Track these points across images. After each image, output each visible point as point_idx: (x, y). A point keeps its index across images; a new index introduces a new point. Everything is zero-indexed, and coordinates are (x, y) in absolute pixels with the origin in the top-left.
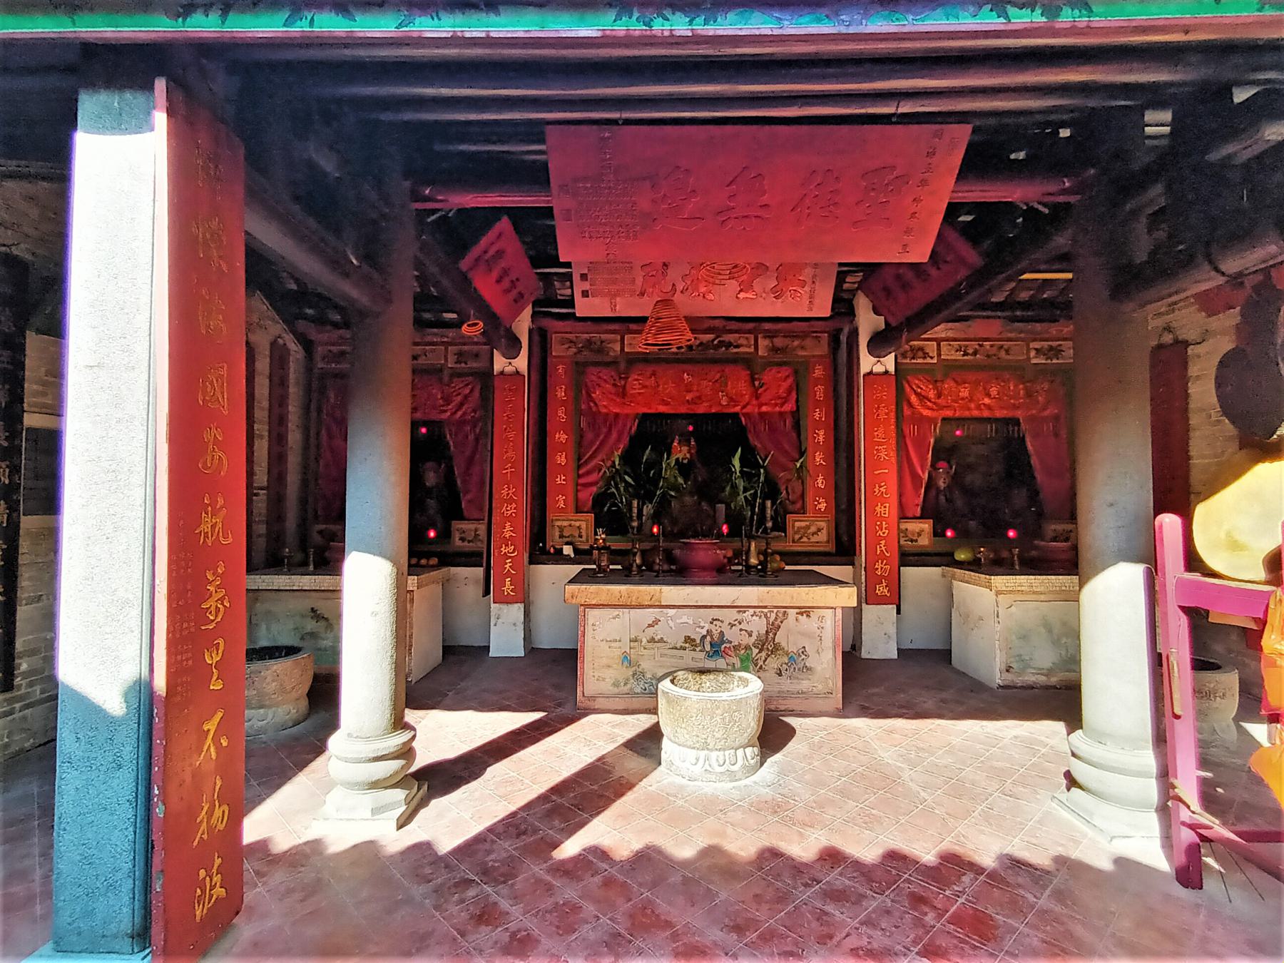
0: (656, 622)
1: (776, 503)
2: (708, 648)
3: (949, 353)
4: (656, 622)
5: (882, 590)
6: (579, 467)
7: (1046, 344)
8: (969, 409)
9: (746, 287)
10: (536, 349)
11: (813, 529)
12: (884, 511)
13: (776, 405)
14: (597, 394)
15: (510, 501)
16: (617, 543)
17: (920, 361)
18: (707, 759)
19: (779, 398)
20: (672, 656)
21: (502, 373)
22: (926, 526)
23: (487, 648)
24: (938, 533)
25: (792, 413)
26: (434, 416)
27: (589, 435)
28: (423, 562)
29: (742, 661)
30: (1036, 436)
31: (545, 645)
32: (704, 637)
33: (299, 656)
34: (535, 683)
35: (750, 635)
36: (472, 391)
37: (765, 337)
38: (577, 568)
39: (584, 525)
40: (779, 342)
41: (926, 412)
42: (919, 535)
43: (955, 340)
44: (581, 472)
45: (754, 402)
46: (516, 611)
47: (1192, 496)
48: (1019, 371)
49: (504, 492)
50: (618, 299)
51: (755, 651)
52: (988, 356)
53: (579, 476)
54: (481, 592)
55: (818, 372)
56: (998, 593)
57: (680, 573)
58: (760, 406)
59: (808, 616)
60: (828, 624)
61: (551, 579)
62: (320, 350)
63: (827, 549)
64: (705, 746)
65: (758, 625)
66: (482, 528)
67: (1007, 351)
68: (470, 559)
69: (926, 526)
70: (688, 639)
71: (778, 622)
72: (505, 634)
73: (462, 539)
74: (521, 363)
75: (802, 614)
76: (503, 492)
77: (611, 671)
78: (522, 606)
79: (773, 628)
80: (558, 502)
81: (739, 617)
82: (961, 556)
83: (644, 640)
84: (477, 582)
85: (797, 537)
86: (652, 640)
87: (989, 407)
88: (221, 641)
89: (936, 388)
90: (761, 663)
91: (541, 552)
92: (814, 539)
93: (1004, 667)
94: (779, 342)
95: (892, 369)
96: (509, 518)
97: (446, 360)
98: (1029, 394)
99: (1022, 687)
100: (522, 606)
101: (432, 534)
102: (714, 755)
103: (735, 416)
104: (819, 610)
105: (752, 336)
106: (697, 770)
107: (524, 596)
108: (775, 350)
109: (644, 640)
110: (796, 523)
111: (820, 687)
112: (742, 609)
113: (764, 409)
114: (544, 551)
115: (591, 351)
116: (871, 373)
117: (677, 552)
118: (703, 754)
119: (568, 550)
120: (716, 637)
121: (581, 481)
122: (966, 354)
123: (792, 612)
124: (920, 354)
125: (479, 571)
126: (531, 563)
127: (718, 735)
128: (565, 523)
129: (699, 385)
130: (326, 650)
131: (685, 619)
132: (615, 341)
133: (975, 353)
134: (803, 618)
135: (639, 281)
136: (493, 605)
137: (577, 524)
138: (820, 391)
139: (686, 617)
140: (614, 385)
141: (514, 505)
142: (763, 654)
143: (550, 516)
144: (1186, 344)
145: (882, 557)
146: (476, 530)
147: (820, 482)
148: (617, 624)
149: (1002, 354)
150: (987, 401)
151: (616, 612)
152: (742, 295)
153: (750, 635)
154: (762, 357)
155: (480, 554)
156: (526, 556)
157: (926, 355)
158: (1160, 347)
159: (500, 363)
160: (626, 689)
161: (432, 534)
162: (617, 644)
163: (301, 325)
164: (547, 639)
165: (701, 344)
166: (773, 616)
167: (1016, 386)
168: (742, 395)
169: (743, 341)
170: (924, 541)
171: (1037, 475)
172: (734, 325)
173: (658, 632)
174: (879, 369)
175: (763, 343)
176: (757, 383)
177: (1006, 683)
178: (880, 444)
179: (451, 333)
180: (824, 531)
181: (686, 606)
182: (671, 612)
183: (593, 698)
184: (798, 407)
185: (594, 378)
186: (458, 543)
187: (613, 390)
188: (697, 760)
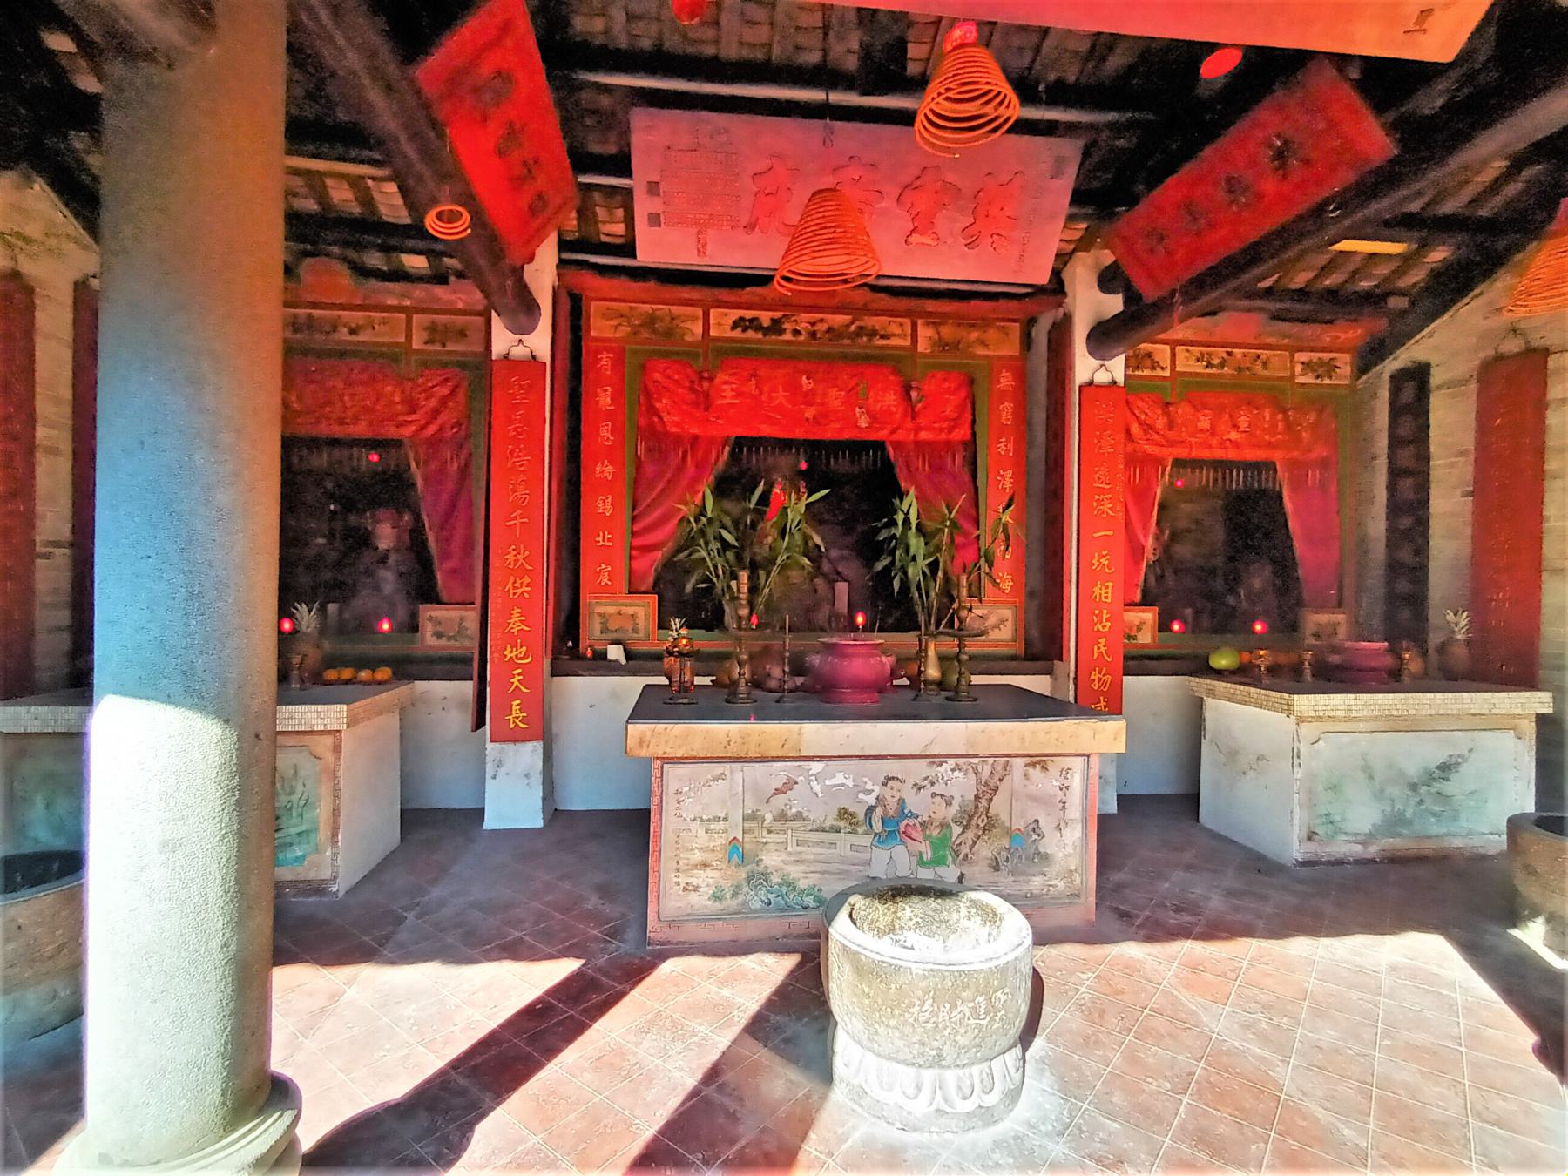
0: (790, 785)
2: (877, 826)
3: (1187, 362)
4: (790, 785)
6: (634, 519)
7: (1315, 356)
8: (1210, 447)
9: (922, 225)
10: (564, 324)
11: (993, 620)
12: (1104, 597)
13: (941, 430)
14: (663, 404)
16: (706, 641)
17: (1146, 372)
18: (940, 1086)
19: (946, 419)
20: (817, 844)
21: (506, 357)
22: (1148, 616)
23: (479, 813)
24: (1163, 626)
25: (964, 443)
26: (390, 431)
27: (649, 470)
28: (364, 675)
29: (935, 848)
30: (1297, 486)
31: (577, 805)
32: (871, 809)
34: (567, 885)
35: (949, 803)
36: (453, 392)
37: (928, 324)
38: (639, 682)
39: (641, 612)
40: (947, 331)
41: (1150, 449)
42: (1139, 629)
43: (1192, 343)
44: (637, 527)
45: (909, 424)
46: (529, 754)
47: (1545, 576)
48: (1274, 396)
50: (710, 231)
51: (957, 830)
53: (634, 534)
54: (469, 718)
55: (1006, 381)
56: (1301, 720)
57: (820, 695)
58: (918, 430)
60: (1076, 782)
61: (595, 702)
63: (1012, 651)
64: (938, 1062)
65: (961, 786)
66: (471, 617)
67: (1265, 364)
68: (449, 667)
69: (1148, 616)
70: (844, 814)
71: (992, 783)
72: (511, 797)
73: (439, 635)
74: (540, 342)
75: (1033, 765)
76: (506, 557)
77: (709, 872)
78: (539, 745)
79: (988, 791)
80: (598, 572)
81: (932, 772)
82: (1221, 661)
83: (769, 817)
84: (461, 705)
87: (1236, 445)
89: (1167, 414)
90: (965, 850)
91: (570, 649)
92: (994, 635)
93: (1304, 834)
94: (947, 331)
95: (1120, 379)
96: (520, 601)
97: (409, 336)
98: (1289, 427)
99: (1329, 863)
100: (539, 745)
101: (386, 626)
102: (951, 1076)
103: (879, 446)
104: (1070, 766)
105: (907, 322)
106: (920, 1107)
107: (541, 729)
108: (942, 345)
109: (769, 817)
111: (1061, 885)
112: (937, 759)
113: (923, 435)
114: (575, 654)
115: (654, 331)
116: (1091, 383)
117: (815, 660)
118: (928, 1075)
119: (615, 653)
120: (892, 807)
121: (638, 542)
123: (1020, 762)
124: (1148, 362)
125: (467, 688)
126: (555, 673)
127: (962, 1040)
128: (611, 610)
129: (825, 394)
131: (840, 778)
132: (694, 318)
133: (1223, 364)
134: (1036, 773)
135: (747, 201)
136: (489, 746)
137: (631, 610)
138: (1006, 411)
139: (841, 776)
140: (692, 390)
141: (527, 580)
142: (970, 835)
143: (586, 598)
144: (1546, 352)
146: (462, 619)
148: (733, 796)
149: (1258, 368)
150: (1234, 435)
151: (717, 769)
152: (915, 238)
153: (949, 803)
154: (924, 355)
155: (466, 661)
156: (547, 663)
158: (1500, 358)
159: (503, 341)
160: (731, 903)
161: (386, 626)
162: (721, 826)
164: (581, 796)
165: (830, 330)
166: (987, 770)
167: (1273, 416)
168: (891, 413)
169: (895, 329)
170: (1145, 638)
171: (1297, 545)
172: (884, 301)
173: (796, 802)
174: (1102, 377)
175: (925, 333)
176: (914, 394)
177: (1309, 857)
178: (1102, 491)
179: (419, 292)
180: (1010, 624)
181: (841, 757)
182: (816, 767)
183: (675, 923)
184: (974, 435)
185: (657, 376)
186: (430, 640)
187: (691, 397)
188: (919, 1088)
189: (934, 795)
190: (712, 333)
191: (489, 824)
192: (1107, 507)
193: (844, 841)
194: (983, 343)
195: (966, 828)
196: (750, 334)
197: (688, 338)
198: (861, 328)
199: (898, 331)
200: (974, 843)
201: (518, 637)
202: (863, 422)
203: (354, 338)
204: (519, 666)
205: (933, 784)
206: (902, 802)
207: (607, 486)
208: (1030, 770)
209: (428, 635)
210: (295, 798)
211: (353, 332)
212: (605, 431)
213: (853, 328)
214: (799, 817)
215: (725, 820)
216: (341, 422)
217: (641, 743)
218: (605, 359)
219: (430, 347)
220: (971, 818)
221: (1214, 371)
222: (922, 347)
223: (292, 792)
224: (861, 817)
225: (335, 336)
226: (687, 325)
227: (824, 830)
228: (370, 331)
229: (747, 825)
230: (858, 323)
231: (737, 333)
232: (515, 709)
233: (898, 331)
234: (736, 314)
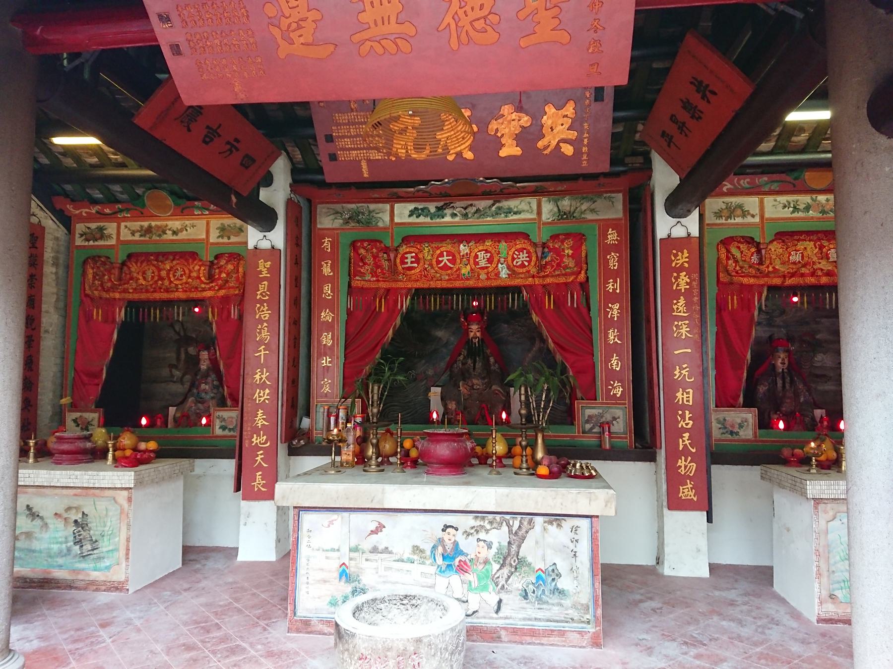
0: (380, 528)
1: (570, 390)
5: (687, 492)
15: (263, 386)
17: (739, 220)
22: (749, 416)
24: (764, 423)
29: (479, 579)
33: (504, 601)
35: (490, 546)
49: (257, 377)
51: (496, 566)
52: (823, 212)
59: (559, 526)
62: (80, 227)
69: (749, 416)
70: (416, 549)
73: (223, 428)
74: (277, 237)
75: (551, 523)
85: (588, 426)
86: (375, 550)
88: (694, 451)
90: (502, 582)
110: (587, 411)
120: (449, 546)
122: (796, 209)
123: (539, 520)
130: (40, 552)
133: (808, 208)
134: (553, 529)
142: (506, 571)
145: (686, 452)
147: (615, 363)
153: (490, 546)
157: (745, 214)
162: (336, 554)
163: (60, 202)
173: (381, 540)
174: (679, 232)
178: (682, 318)
189: (479, 540)
190: (397, 220)
191: (242, 557)
192: (684, 330)
193: (417, 569)
194: (593, 211)
195: (502, 566)
196: (422, 219)
197: (380, 224)
198: (499, 208)
199: (526, 207)
200: (509, 577)
201: (261, 430)
202: (504, 273)
203: (175, 237)
204: (261, 448)
205: (477, 532)
206: (456, 544)
207: (329, 327)
208: (549, 527)
209: (217, 427)
210: (107, 529)
211: (175, 233)
212: (327, 289)
213: (494, 208)
214: (386, 550)
215: (338, 550)
216: (167, 291)
217: (283, 497)
218: (327, 243)
219: (220, 240)
220: (505, 559)
221: (801, 214)
222: (545, 217)
223: (105, 526)
224: (428, 553)
225: (165, 237)
226: (380, 215)
227: (403, 561)
228: (185, 232)
229: (353, 555)
230: (497, 205)
231: (413, 219)
232: (258, 477)
233: (526, 207)
234: (411, 206)
